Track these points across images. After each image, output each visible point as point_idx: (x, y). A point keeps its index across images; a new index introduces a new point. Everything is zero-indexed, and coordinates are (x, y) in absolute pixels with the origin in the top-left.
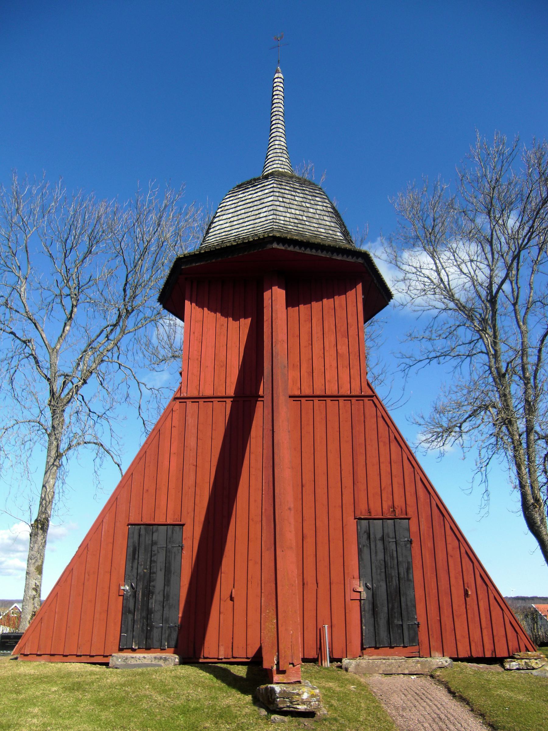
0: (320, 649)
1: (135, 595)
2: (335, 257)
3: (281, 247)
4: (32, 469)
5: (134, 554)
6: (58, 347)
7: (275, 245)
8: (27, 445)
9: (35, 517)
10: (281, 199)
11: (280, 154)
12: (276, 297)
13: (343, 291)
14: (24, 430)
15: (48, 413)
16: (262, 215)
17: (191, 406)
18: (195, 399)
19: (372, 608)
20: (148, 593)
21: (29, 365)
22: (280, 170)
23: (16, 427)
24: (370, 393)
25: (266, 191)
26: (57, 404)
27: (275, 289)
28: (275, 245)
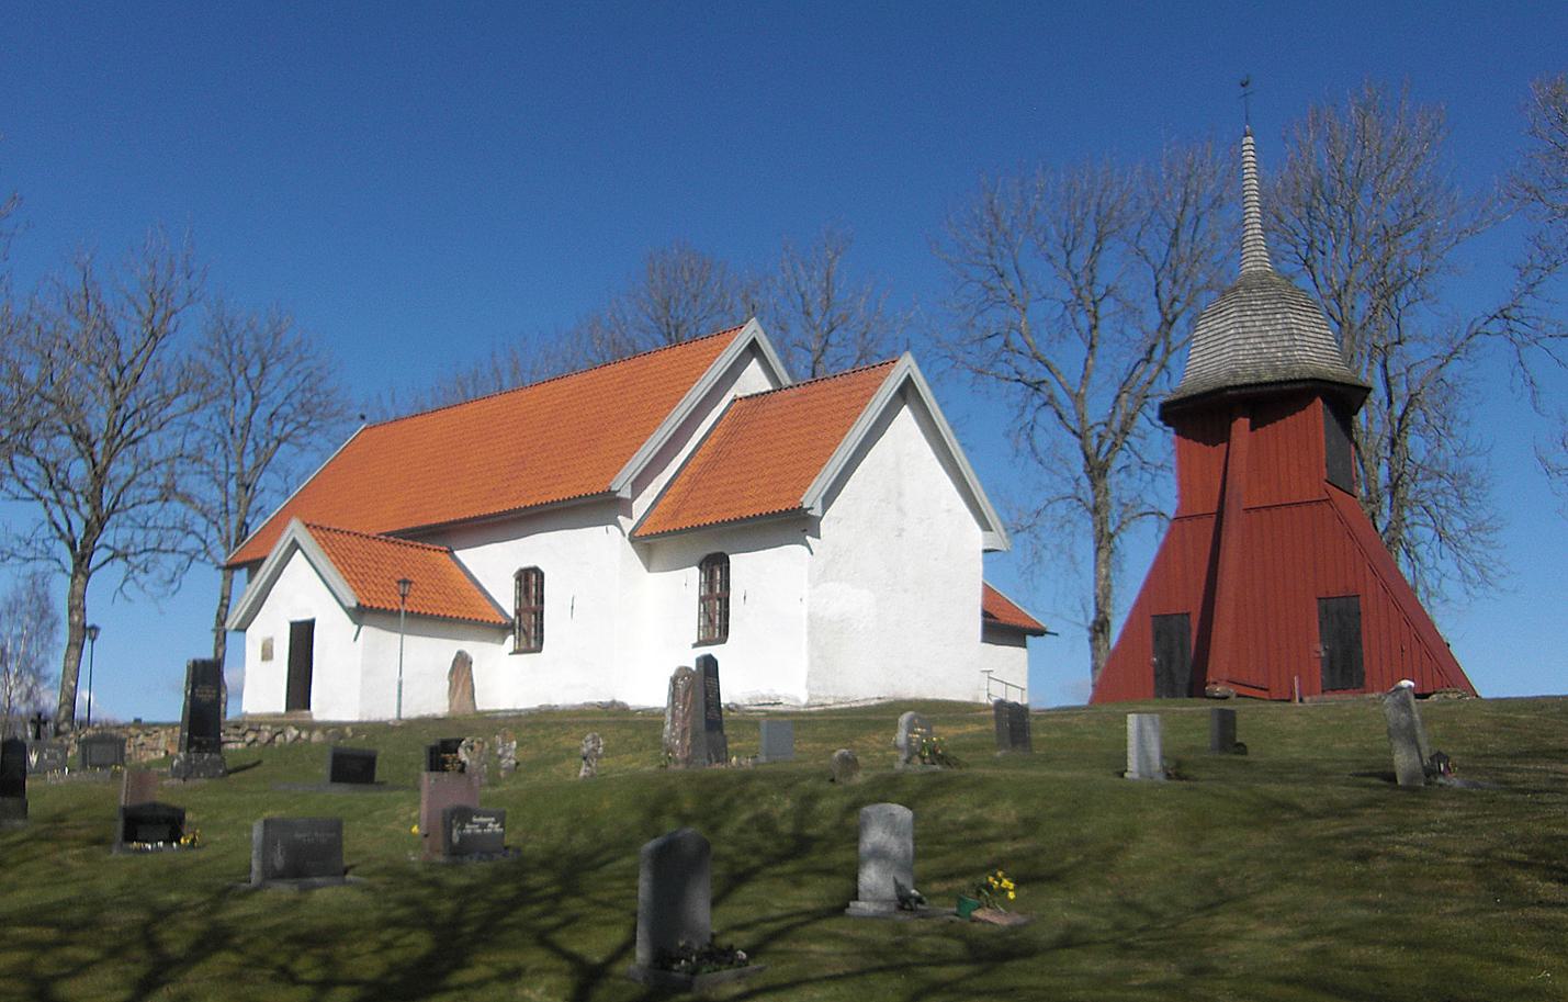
0: (1292, 693)
1: (1161, 665)
2: (1285, 387)
3: (1234, 392)
4: (1079, 558)
5: (1157, 636)
6: (1082, 391)
7: (1229, 392)
8: (1068, 528)
9: (1092, 617)
10: (1241, 330)
11: (1253, 248)
12: (1242, 424)
13: (1312, 401)
14: (1061, 509)
15: (1085, 482)
16: (1224, 351)
17: (1186, 522)
18: (1189, 517)
19: (1330, 663)
20: (1170, 662)
21: (1047, 417)
22: (1253, 269)
23: (1050, 508)
24: (1327, 497)
25: (1230, 322)
26: (1097, 471)
27: (1241, 419)
28: (1229, 392)
